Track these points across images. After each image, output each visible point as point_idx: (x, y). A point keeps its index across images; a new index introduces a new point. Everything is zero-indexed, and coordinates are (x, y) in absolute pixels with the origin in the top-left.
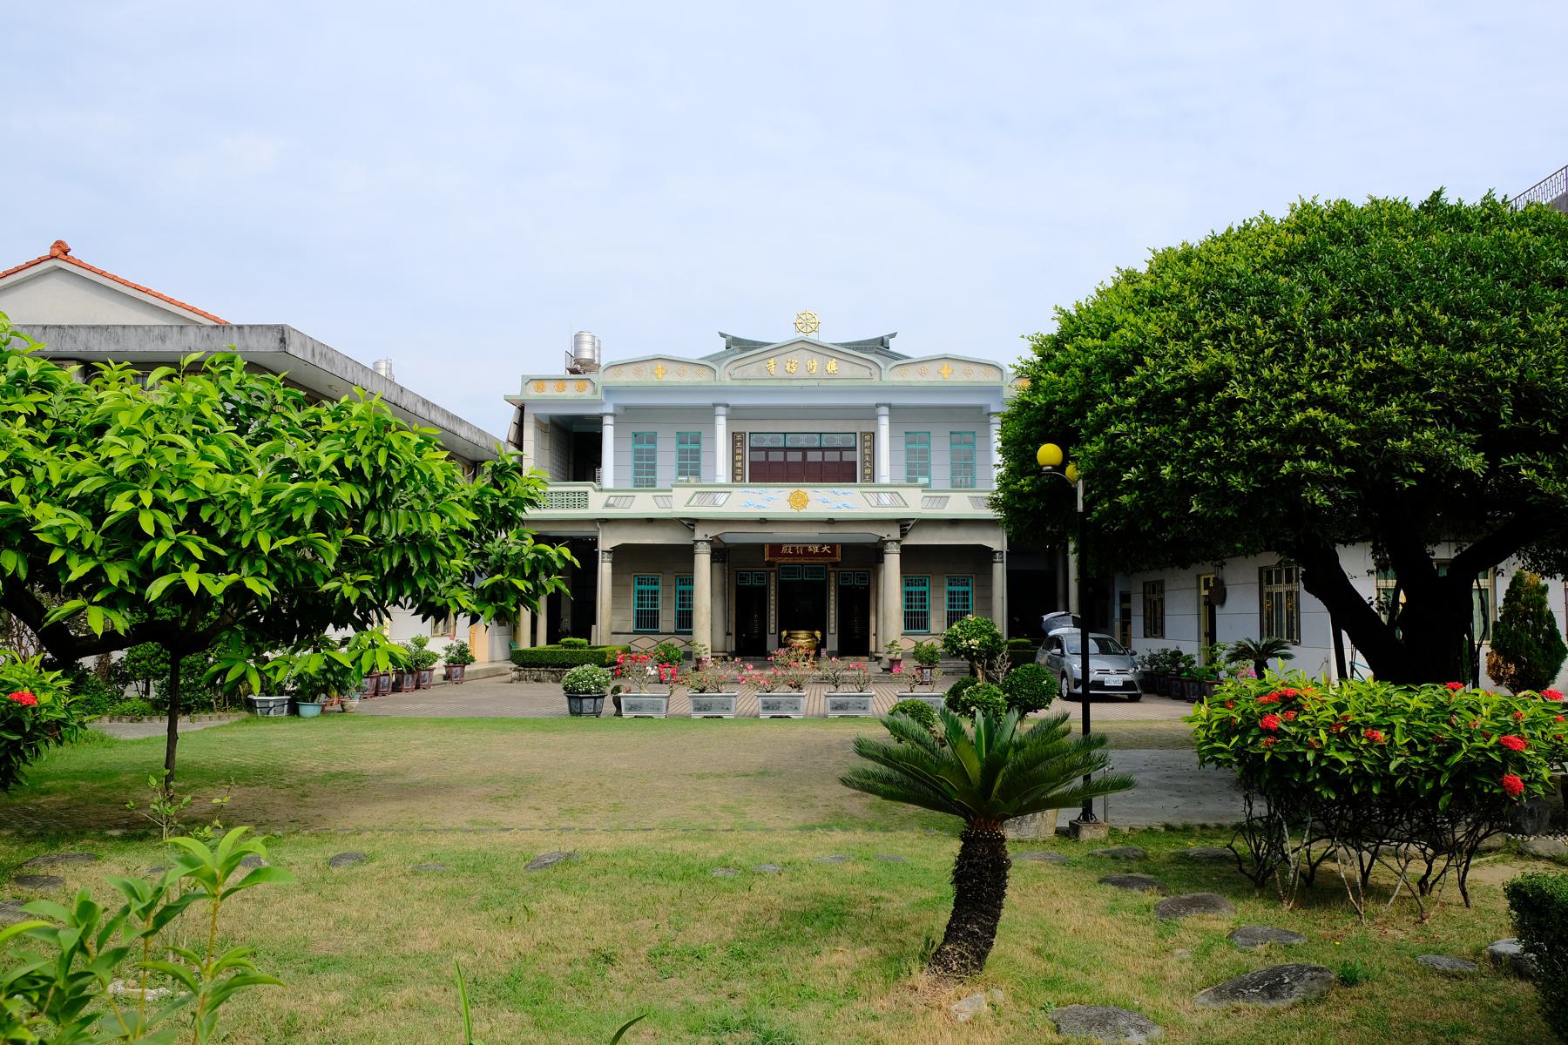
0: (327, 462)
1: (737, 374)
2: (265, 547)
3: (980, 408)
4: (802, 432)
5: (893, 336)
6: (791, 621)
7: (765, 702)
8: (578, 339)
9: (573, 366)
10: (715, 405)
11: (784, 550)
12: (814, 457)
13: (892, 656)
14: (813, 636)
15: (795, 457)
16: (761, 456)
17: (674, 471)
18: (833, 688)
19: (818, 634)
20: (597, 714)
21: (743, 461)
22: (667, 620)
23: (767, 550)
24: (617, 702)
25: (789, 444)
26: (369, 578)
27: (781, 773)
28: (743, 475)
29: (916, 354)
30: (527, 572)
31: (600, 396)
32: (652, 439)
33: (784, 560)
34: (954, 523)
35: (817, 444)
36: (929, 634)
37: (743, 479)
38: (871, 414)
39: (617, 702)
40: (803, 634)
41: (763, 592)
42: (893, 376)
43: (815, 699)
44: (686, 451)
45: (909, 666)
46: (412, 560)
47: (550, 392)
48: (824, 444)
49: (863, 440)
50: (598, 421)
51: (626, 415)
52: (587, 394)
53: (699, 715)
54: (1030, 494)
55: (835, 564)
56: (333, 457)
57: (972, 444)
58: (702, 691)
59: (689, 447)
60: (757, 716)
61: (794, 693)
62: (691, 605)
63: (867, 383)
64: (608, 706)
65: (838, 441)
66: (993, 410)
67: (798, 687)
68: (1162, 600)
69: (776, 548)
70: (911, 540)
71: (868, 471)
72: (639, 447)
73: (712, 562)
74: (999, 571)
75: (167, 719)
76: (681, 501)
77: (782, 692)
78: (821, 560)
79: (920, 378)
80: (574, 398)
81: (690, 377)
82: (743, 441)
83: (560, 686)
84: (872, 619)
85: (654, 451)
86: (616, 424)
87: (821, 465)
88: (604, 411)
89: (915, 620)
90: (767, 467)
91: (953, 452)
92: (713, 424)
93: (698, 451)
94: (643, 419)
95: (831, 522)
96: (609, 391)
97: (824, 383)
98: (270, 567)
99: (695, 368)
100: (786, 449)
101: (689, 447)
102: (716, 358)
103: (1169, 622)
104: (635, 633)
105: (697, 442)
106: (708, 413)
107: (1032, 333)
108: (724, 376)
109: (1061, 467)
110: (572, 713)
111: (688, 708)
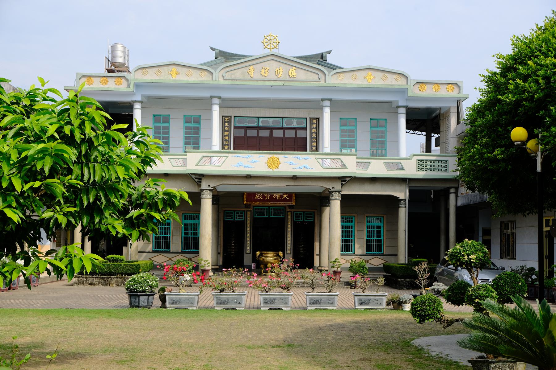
0: (52, 130)
1: (227, 76)
2: (18, 188)
3: (391, 103)
4: (270, 116)
5: (329, 52)
6: (261, 245)
7: (265, 299)
8: (113, 49)
9: (109, 68)
10: (212, 97)
11: (257, 197)
12: (278, 134)
13: (335, 269)
14: (278, 255)
15: (265, 134)
16: (241, 133)
17: (181, 142)
18: (311, 290)
19: (281, 254)
20: (149, 306)
21: (229, 136)
22: (176, 243)
23: (245, 196)
24: (163, 299)
25: (261, 125)
26: (72, 209)
27: (301, 345)
28: (229, 145)
29: (347, 66)
30: (160, 207)
31: (132, 88)
32: (166, 119)
33: (257, 203)
34: (373, 180)
35: (280, 125)
36: (354, 254)
37: (229, 148)
38: (318, 105)
39: (163, 299)
40: (271, 254)
41: (242, 225)
42: (333, 80)
43: (298, 297)
44: (190, 128)
45: (346, 276)
46: (103, 199)
47: (97, 85)
48: (285, 125)
49: (311, 123)
50: (130, 106)
51: (149, 102)
52: (123, 87)
53: (219, 308)
54: (503, 159)
55: (291, 207)
56: (56, 126)
57: (385, 127)
58: (221, 291)
59: (192, 125)
60: (259, 308)
61: (285, 292)
62: (197, 234)
63: (316, 84)
64: (157, 302)
65: (294, 124)
66: (400, 104)
67: (287, 288)
68: (514, 235)
69: (251, 195)
70: (346, 191)
71: (314, 144)
72: (158, 124)
73: (213, 204)
74: (403, 213)
75: (403, 305)
76: (193, 163)
77: (275, 292)
78: (281, 204)
79: (352, 82)
80: (114, 89)
81: (195, 77)
82: (229, 122)
83: (123, 289)
84: (317, 245)
85: (167, 128)
86: (143, 108)
87: (283, 139)
88: (135, 99)
89: (347, 246)
90: (245, 139)
91: (372, 132)
92: (210, 110)
93: (198, 129)
94: (162, 105)
95: (295, 178)
96: (138, 85)
97: (287, 84)
98: (18, 202)
99: (199, 72)
100: (259, 128)
101: (192, 125)
102: (209, 64)
103: (519, 248)
104: (153, 252)
105: (198, 122)
106: (207, 103)
107: (495, 53)
108: (220, 76)
109: (524, 143)
110: (132, 305)
111: (212, 302)
